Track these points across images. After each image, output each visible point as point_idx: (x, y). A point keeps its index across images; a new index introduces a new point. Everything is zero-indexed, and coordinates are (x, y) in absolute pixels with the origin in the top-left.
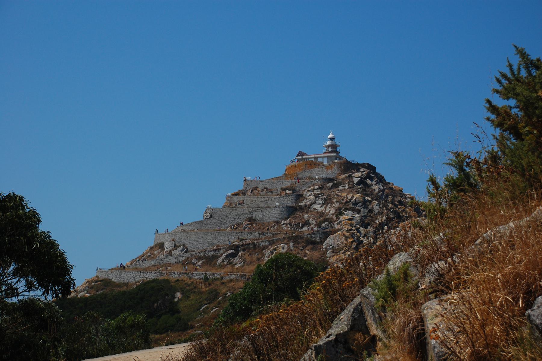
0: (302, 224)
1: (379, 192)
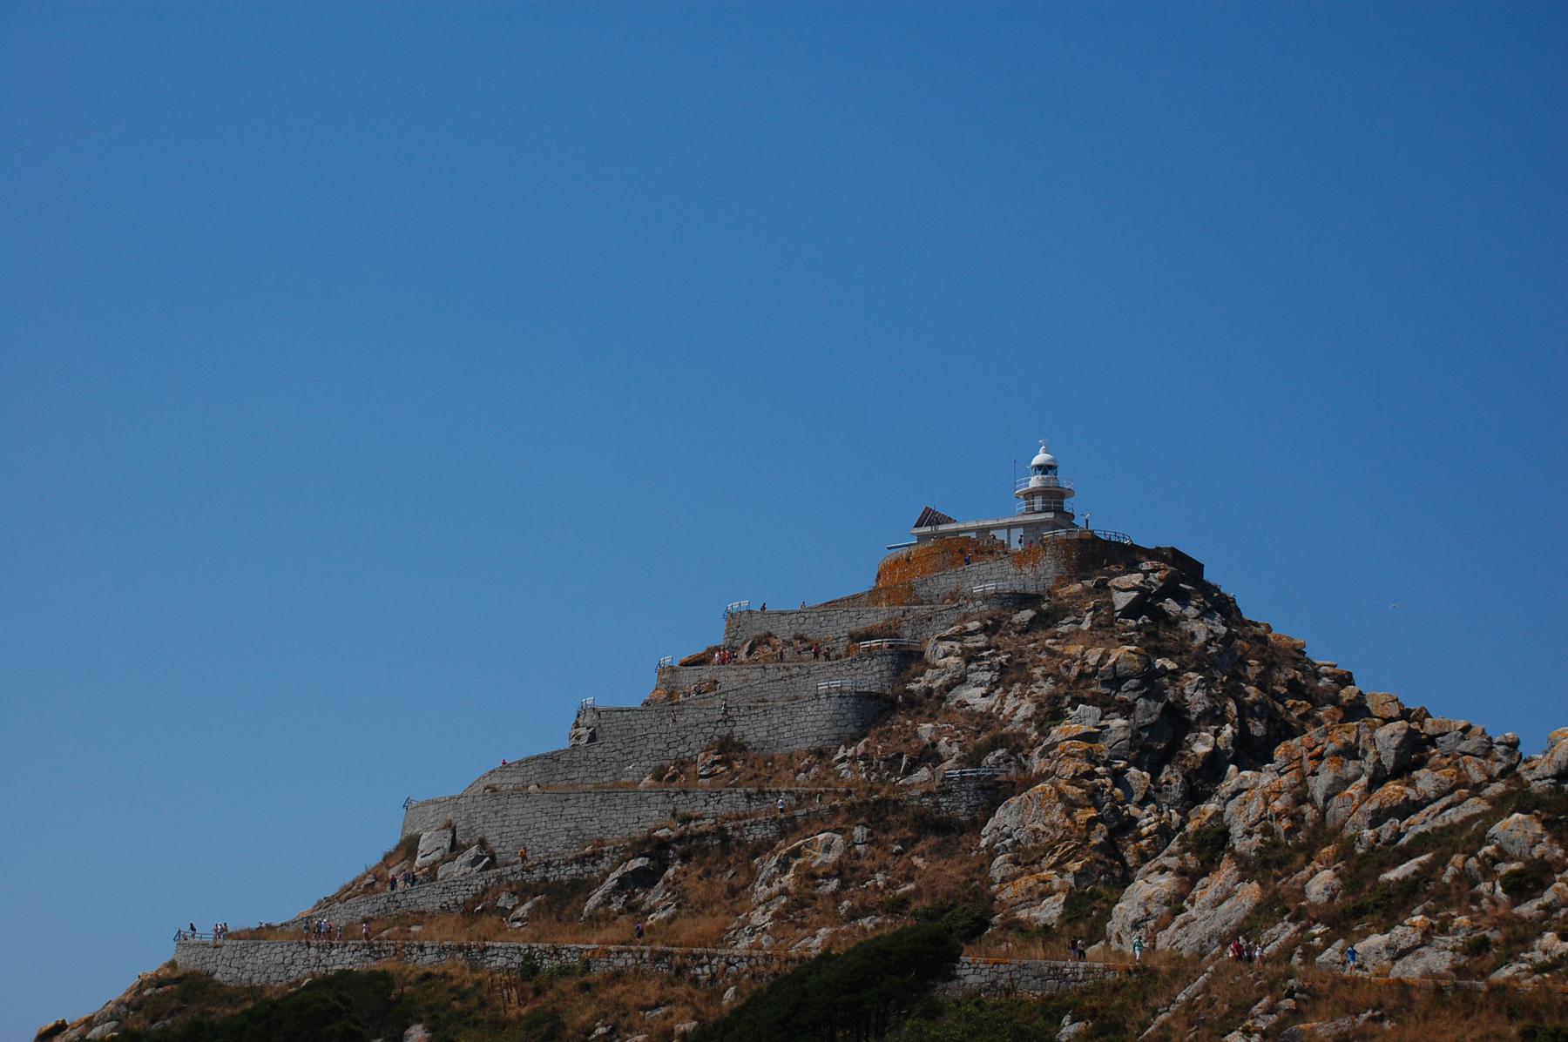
0: (910, 760)
1: (1208, 642)
